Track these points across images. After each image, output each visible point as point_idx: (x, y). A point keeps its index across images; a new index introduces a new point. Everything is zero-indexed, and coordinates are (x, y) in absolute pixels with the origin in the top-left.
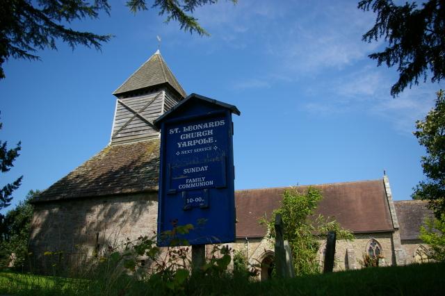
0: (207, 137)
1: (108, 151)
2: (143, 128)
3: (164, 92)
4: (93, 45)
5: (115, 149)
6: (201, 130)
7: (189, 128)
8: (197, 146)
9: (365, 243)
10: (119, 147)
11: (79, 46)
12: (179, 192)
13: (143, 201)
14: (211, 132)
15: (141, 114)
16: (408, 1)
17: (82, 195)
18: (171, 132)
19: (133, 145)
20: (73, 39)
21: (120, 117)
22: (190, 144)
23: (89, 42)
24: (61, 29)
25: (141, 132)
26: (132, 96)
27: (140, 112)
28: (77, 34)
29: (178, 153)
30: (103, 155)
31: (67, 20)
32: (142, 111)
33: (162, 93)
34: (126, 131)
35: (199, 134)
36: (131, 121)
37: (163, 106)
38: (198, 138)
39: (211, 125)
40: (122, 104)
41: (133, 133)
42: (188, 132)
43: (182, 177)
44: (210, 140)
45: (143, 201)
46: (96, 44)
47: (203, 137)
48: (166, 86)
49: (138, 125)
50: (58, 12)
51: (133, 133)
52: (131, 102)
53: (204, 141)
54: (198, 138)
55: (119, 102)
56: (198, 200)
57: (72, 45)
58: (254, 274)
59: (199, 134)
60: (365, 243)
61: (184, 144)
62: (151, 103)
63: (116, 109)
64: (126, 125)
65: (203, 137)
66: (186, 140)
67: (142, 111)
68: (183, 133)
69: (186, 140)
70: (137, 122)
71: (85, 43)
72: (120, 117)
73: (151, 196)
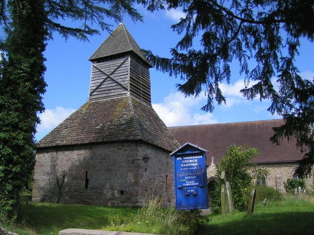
1: (87, 106)
2: (114, 88)
3: (129, 58)
5: (94, 104)
6: (192, 159)
7: (186, 158)
9: (291, 170)
10: (97, 103)
11: (71, 38)
13: (120, 147)
15: (112, 76)
16: (299, 56)
17: (73, 143)
18: (178, 159)
19: (107, 101)
20: (67, 32)
21: (96, 78)
22: (187, 165)
24: (58, 25)
25: (113, 91)
26: (103, 61)
27: (111, 75)
28: (70, 29)
29: (182, 169)
30: (84, 110)
31: (63, 18)
32: (112, 73)
33: (128, 59)
34: (101, 90)
35: (191, 161)
37: (129, 70)
38: (190, 163)
39: (196, 157)
40: (96, 67)
41: (106, 92)
42: (186, 160)
43: (184, 180)
45: (120, 147)
46: (83, 36)
47: (193, 163)
48: (131, 53)
50: (56, 13)
51: (106, 92)
52: (103, 66)
54: (190, 163)
55: (94, 66)
56: (192, 191)
57: (66, 37)
60: (291, 170)
61: (184, 165)
62: (119, 67)
63: (92, 71)
64: (100, 85)
65: (193, 163)
67: (112, 73)
68: (183, 160)
70: (108, 82)
71: (75, 35)
72: (96, 78)
73: (125, 144)
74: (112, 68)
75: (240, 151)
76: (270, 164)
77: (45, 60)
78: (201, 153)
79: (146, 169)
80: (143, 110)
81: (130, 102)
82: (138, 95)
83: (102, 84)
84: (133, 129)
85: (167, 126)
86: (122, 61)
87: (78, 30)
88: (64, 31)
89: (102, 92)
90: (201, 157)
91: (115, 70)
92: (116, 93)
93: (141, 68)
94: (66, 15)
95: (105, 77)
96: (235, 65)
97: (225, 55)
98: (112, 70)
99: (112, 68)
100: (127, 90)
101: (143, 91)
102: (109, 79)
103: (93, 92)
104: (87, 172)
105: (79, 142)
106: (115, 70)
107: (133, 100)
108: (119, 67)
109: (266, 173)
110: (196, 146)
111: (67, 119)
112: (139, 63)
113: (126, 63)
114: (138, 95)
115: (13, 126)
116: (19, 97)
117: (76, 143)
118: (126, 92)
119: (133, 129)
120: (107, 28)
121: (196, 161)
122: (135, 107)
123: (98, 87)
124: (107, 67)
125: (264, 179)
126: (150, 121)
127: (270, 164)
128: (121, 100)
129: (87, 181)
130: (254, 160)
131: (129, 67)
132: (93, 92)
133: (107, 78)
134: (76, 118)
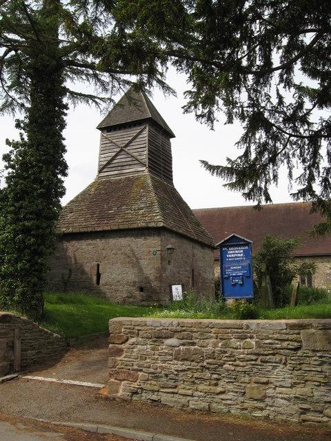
0: (240, 253)
2: (129, 163)
4: (94, 104)
8: (236, 257)
12: (229, 277)
14: (242, 251)
15: (126, 149)
17: (82, 230)
18: (224, 249)
20: (77, 97)
23: (90, 101)
28: (80, 95)
30: (93, 190)
32: (127, 146)
33: (145, 128)
34: (112, 166)
35: (236, 252)
36: (116, 156)
37: (147, 141)
44: (242, 255)
46: (96, 103)
49: (123, 160)
53: (239, 255)
58: (261, 88)
59: (236, 252)
62: (135, 138)
66: (231, 254)
67: (127, 146)
69: (231, 254)
73: (174, 236)
74: (126, 139)
75: (281, 241)
76: (318, 256)
77: (64, 139)
78: (247, 244)
79: (169, 262)
80: (165, 191)
81: (149, 181)
82: (157, 171)
83: (114, 158)
84: (155, 214)
85: (192, 208)
86: (138, 131)
87: (91, 97)
88: (73, 96)
89: (113, 169)
90: (247, 248)
91: (131, 142)
92: (131, 170)
93: (161, 137)
94: (76, 78)
95: (118, 150)
96: (282, 169)
97: (273, 160)
98: (127, 142)
99: (126, 139)
100: (146, 166)
101: (163, 172)
102: (123, 153)
103: (103, 168)
104: (98, 265)
105: (89, 230)
106: (131, 142)
107: (152, 178)
108: (135, 138)
109: (312, 267)
110: (243, 238)
111: (72, 202)
112: (159, 132)
113: (144, 133)
114: (157, 171)
115: (37, 214)
116: (42, 181)
117: (85, 230)
118: (144, 168)
119: (155, 214)
120: (135, 104)
121: (242, 251)
122: (155, 187)
123: (109, 162)
124: (122, 137)
125: (310, 275)
126: (173, 204)
127: (318, 256)
128: (138, 178)
129: (99, 276)
130: (298, 252)
131: (147, 138)
132: (103, 168)
133: (119, 152)
134: (83, 200)
